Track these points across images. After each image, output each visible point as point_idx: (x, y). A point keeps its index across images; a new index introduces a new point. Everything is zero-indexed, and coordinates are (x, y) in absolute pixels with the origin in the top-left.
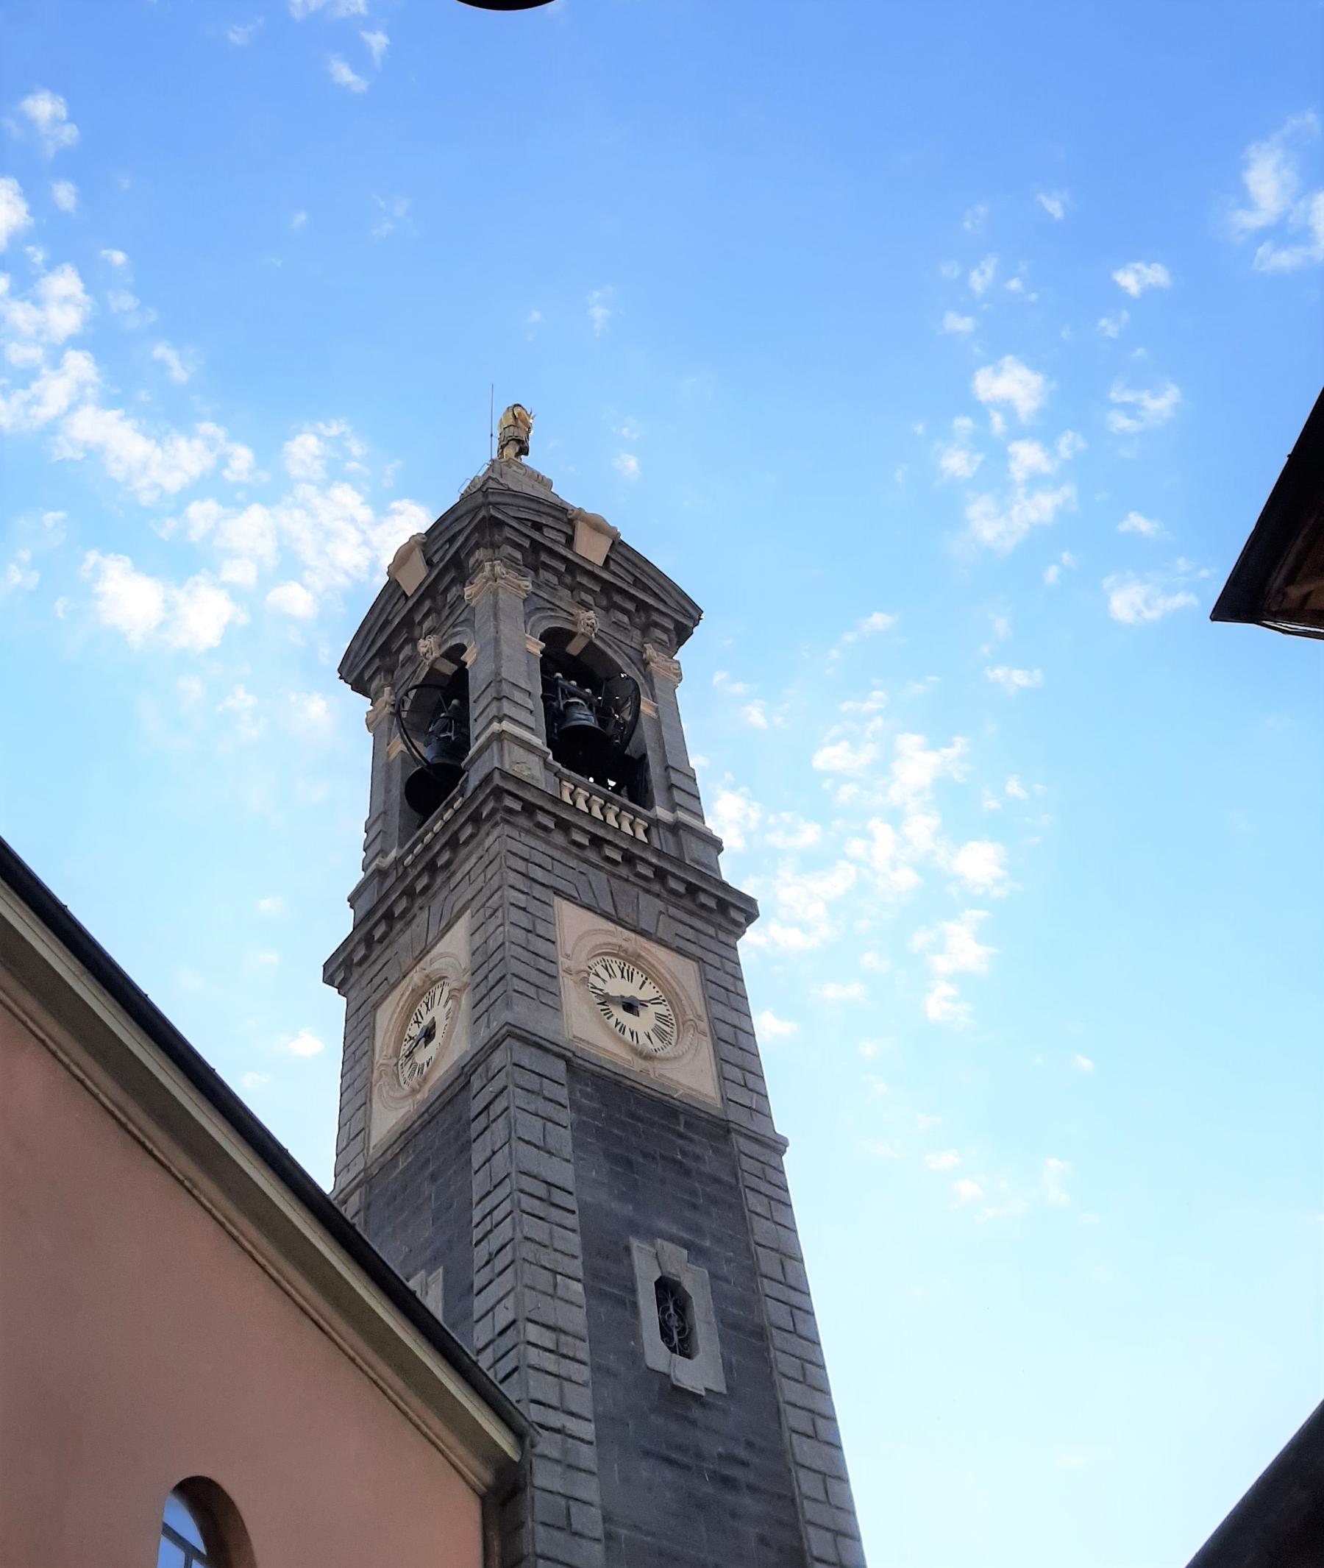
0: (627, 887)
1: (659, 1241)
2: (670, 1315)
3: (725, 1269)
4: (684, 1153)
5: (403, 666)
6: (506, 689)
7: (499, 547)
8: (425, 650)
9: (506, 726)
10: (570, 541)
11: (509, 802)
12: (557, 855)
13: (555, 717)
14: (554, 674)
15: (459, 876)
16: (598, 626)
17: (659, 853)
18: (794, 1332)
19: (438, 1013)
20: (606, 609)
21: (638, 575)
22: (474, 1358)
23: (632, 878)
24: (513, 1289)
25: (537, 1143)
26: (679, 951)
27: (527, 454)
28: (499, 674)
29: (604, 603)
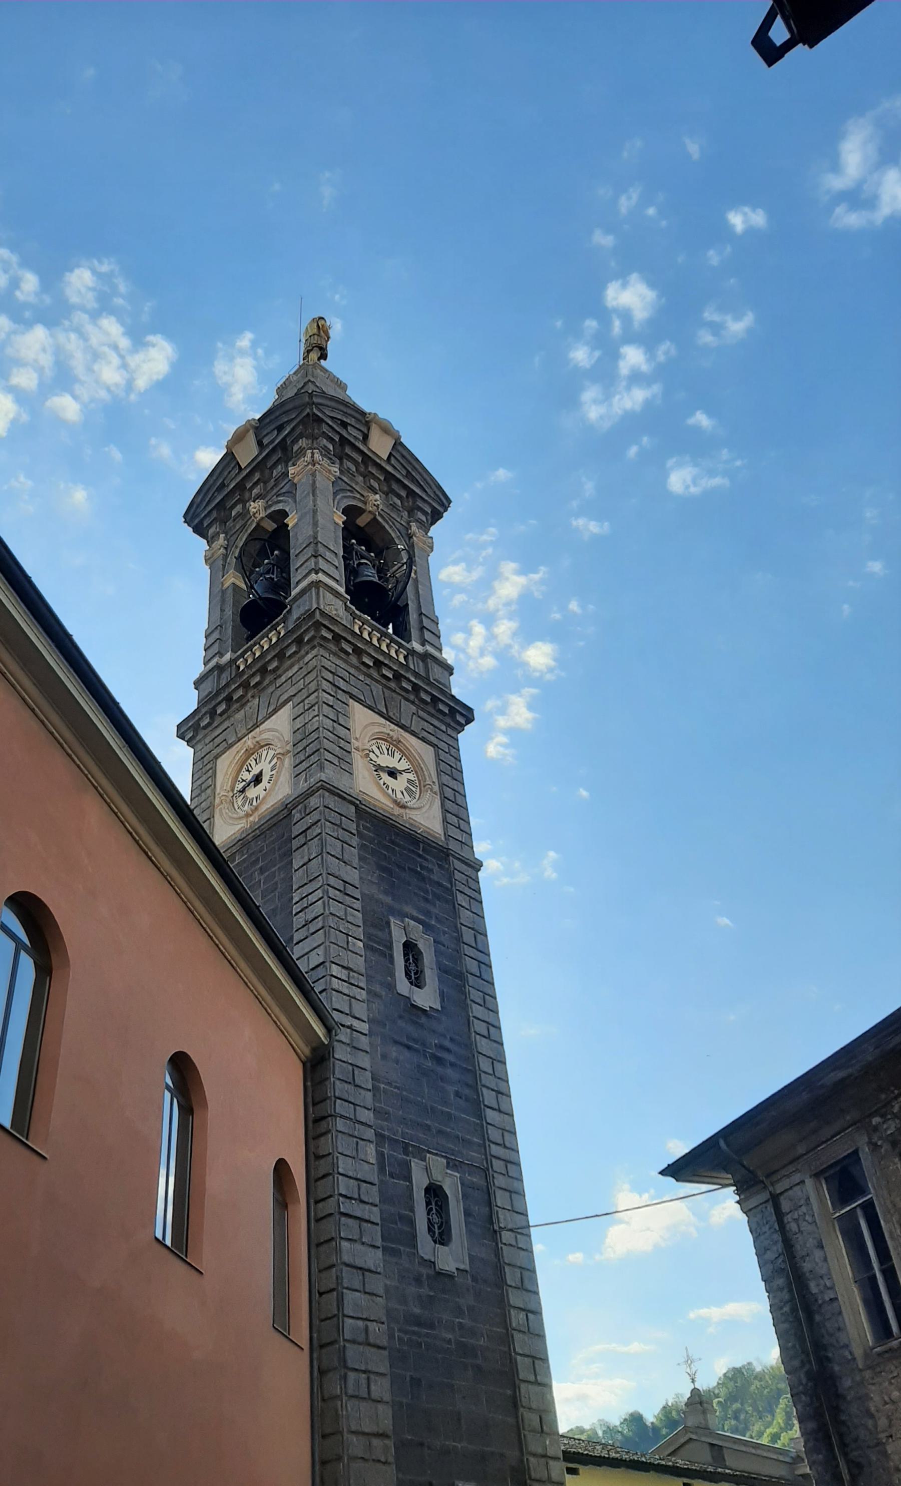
0: (394, 695)
1: (407, 919)
2: (410, 963)
3: (443, 938)
4: (422, 867)
5: (234, 520)
6: (321, 550)
7: (317, 439)
8: (255, 510)
9: (321, 577)
10: (366, 437)
11: (324, 633)
12: (352, 671)
13: (351, 572)
14: (350, 541)
15: (283, 679)
16: (381, 507)
17: (417, 675)
18: (480, 977)
19: (264, 766)
20: (387, 494)
21: (410, 470)
22: (312, 985)
23: (398, 690)
24: (323, 943)
25: (339, 857)
26: (423, 739)
27: (325, 359)
28: (316, 538)
29: (385, 489)
